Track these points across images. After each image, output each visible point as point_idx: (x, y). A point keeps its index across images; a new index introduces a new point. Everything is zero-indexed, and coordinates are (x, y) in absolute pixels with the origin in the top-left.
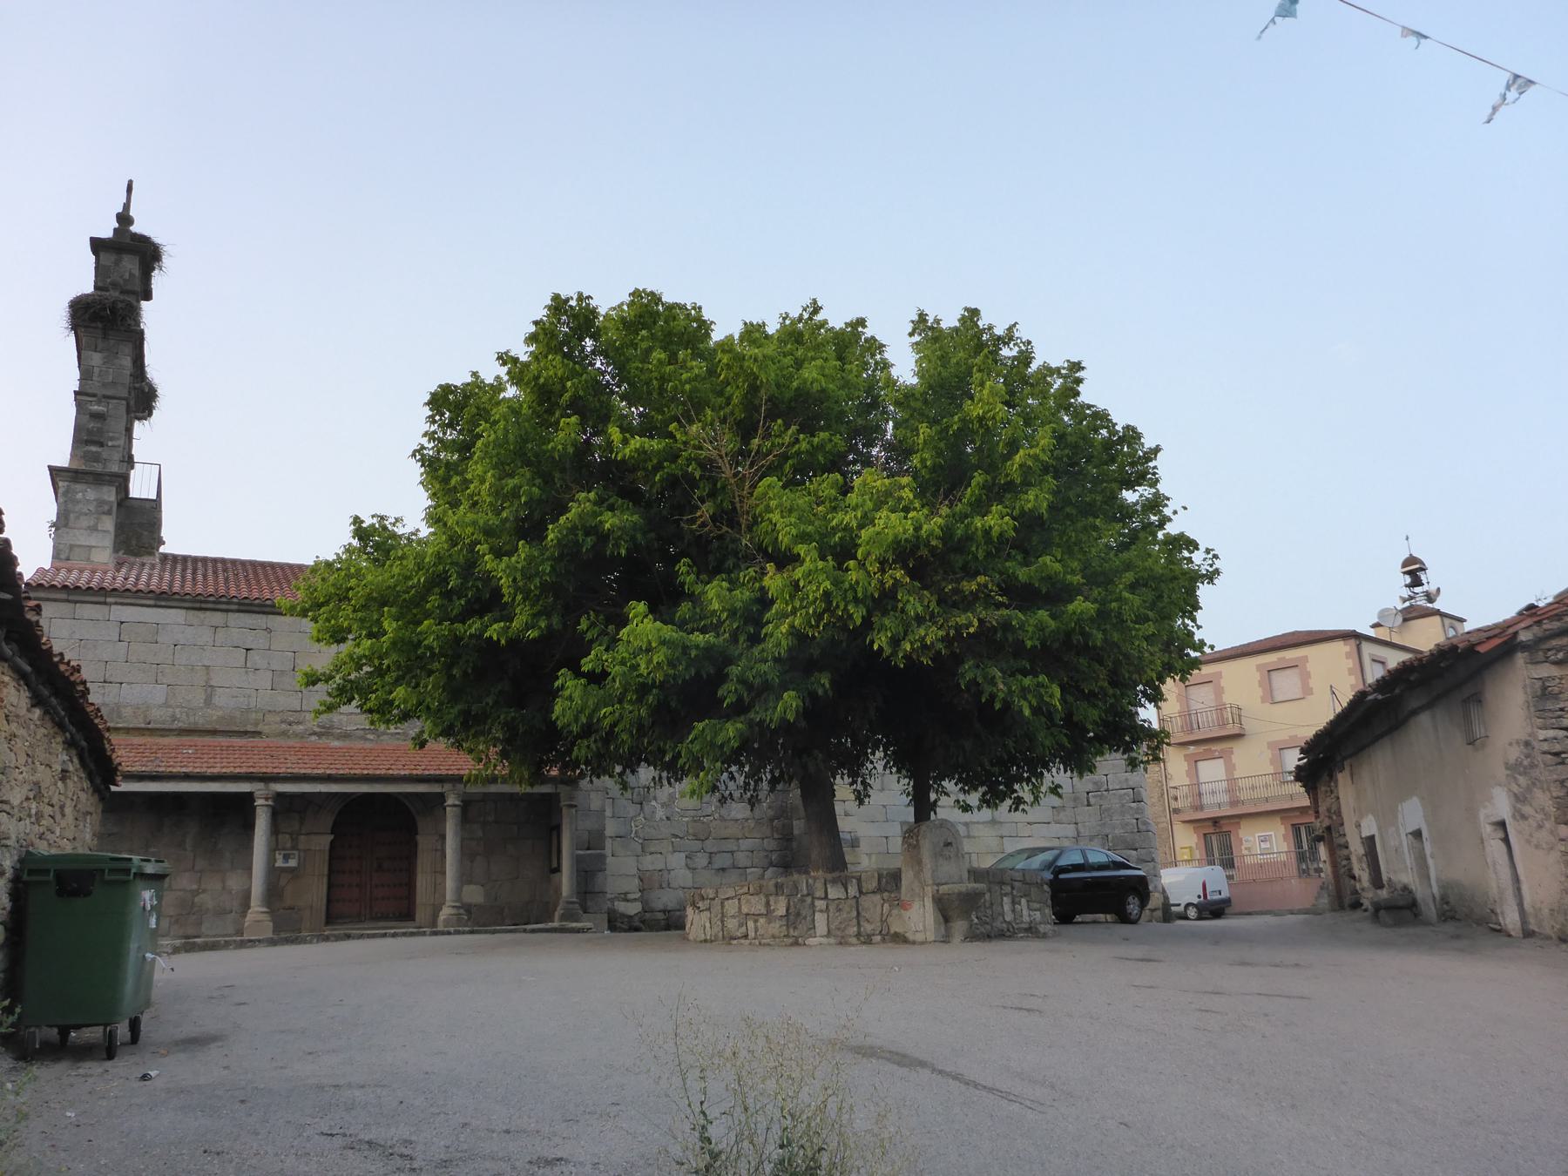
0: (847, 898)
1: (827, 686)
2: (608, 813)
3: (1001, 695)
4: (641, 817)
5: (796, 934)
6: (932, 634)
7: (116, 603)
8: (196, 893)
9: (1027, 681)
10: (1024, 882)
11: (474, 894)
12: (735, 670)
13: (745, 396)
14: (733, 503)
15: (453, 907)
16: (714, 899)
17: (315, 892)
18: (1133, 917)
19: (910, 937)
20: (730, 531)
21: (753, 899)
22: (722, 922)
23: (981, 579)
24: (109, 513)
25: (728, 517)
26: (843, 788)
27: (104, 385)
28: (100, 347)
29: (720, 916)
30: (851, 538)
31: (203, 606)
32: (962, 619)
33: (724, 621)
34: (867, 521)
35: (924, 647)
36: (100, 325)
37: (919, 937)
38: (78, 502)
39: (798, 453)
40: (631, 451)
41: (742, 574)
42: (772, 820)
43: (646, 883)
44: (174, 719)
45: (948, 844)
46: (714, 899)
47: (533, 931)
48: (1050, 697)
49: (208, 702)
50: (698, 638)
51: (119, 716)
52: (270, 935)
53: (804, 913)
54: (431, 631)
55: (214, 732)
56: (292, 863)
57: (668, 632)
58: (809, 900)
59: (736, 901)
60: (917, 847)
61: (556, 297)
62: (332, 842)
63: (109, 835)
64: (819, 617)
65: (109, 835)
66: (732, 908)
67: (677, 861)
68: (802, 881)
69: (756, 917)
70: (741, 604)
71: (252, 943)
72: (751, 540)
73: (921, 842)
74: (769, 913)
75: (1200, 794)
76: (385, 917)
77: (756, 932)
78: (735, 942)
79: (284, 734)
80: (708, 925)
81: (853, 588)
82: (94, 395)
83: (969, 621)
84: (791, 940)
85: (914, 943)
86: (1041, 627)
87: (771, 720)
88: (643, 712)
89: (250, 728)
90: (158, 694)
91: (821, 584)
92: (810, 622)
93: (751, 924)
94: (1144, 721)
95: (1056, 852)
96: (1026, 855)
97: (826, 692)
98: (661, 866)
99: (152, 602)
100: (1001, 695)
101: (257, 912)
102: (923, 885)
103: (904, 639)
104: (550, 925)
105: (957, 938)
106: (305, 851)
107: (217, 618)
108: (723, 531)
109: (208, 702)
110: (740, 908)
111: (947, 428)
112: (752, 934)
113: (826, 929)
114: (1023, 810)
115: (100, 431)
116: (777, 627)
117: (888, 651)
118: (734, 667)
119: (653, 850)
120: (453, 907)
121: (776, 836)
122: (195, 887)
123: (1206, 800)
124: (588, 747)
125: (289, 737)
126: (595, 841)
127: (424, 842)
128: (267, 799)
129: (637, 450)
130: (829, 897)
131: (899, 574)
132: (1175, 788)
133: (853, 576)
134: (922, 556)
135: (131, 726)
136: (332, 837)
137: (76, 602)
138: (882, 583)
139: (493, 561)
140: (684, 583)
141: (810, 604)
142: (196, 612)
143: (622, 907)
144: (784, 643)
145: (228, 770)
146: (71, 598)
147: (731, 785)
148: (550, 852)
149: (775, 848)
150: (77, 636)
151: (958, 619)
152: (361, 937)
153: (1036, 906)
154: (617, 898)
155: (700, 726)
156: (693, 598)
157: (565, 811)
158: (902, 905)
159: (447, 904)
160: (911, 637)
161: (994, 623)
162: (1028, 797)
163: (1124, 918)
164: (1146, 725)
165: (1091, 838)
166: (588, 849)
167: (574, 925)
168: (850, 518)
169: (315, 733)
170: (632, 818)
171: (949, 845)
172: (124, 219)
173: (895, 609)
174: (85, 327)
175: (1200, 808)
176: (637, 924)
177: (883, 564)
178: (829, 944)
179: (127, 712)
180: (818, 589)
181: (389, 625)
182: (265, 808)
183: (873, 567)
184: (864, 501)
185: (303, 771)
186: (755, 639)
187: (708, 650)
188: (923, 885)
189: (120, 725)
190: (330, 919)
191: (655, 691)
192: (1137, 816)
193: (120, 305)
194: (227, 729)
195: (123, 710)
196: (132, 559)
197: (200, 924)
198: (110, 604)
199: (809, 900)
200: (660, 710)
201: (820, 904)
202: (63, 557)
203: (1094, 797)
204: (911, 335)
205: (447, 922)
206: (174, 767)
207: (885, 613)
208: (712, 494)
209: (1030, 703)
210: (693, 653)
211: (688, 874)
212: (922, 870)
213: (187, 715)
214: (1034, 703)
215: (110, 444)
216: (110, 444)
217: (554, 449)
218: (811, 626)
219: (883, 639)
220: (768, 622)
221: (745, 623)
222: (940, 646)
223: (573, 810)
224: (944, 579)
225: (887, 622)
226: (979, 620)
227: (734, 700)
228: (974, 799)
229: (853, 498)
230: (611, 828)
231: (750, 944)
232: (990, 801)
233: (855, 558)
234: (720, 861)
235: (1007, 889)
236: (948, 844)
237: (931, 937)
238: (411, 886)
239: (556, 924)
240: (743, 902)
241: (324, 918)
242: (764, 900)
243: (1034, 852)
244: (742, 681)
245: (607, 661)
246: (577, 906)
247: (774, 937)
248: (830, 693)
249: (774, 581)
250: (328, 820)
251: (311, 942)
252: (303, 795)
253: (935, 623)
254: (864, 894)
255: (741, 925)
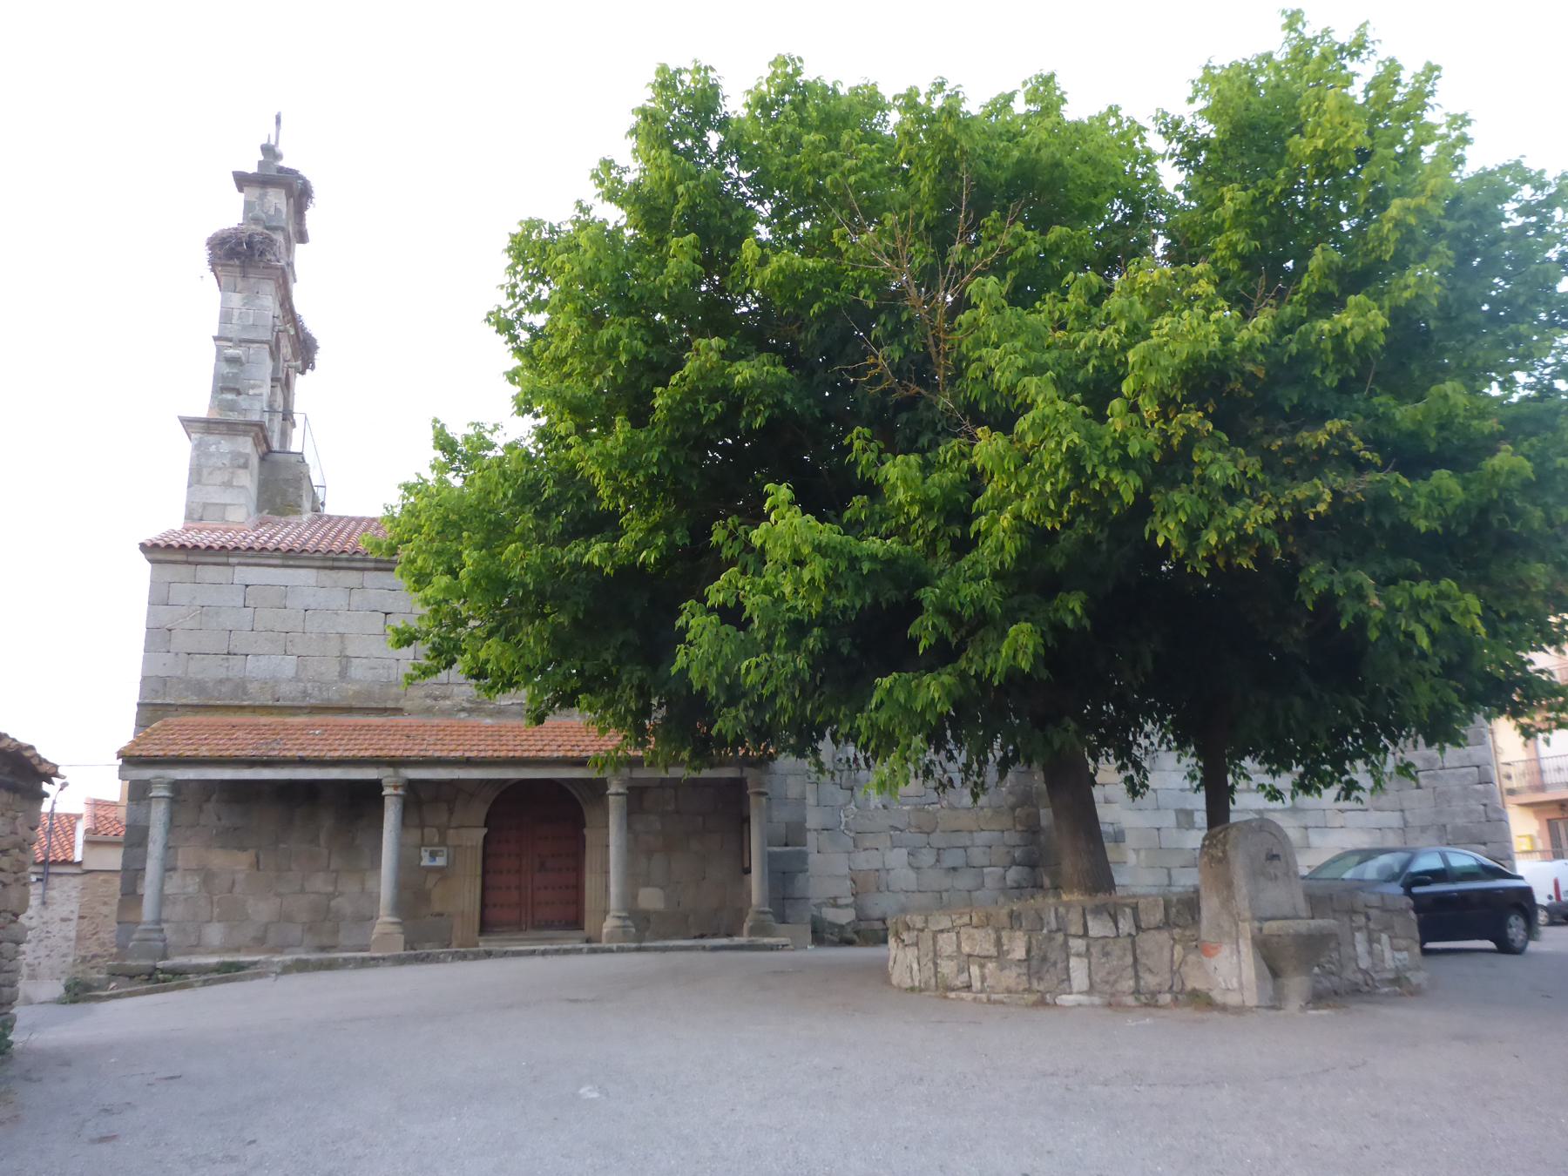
0: (1118, 936)
1: (1078, 611)
2: (811, 800)
3: (1377, 615)
4: (852, 806)
5: (1041, 988)
6: (1255, 516)
7: (240, 564)
8: (331, 896)
9: (1423, 590)
10: (1384, 909)
11: (651, 899)
12: (928, 595)
13: (937, 181)
14: (925, 346)
15: (619, 917)
16: (922, 930)
17: (466, 896)
18: (1517, 945)
19: (1218, 996)
20: (923, 391)
21: (978, 934)
22: (936, 964)
23: (1333, 425)
24: (245, 466)
25: (919, 368)
26: (1108, 776)
27: (245, 328)
28: (239, 288)
29: (931, 955)
30: (1111, 367)
31: (336, 564)
32: (1302, 491)
33: (916, 519)
34: (1137, 332)
35: (1243, 539)
36: (237, 262)
37: (1233, 999)
38: (212, 455)
39: (1025, 258)
40: (772, 272)
41: (941, 449)
42: (1013, 809)
43: (861, 885)
44: (305, 694)
45: (1273, 857)
46: (922, 930)
47: (715, 949)
48: (1462, 615)
49: (343, 674)
50: (874, 545)
51: (245, 693)
52: (400, 951)
53: (1052, 956)
54: (517, 558)
55: (349, 710)
56: (440, 861)
57: (828, 533)
58: (1060, 937)
59: (953, 935)
60: (1223, 860)
61: (663, 69)
62: (485, 837)
63: (235, 829)
64: (1063, 497)
65: (235, 829)
66: (947, 943)
67: (898, 858)
68: (1047, 904)
69: (983, 959)
70: (938, 492)
71: (374, 962)
72: (953, 398)
73: (1231, 854)
74: (1001, 955)
75: (1541, 772)
76: (549, 925)
77: (983, 982)
78: (952, 995)
79: (428, 711)
80: (915, 966)
81: (1121, 443)
82: (230, 340)
83: (1318, 494)
84: (1031, 998)
85: (1224, 1008)
86: (1438, 499)
87: (993, 672)
88: (801, 663)
89: (390, 704)
90: (288, 666)
91: (1062, 438)
92: (1047, 507)
93: (975, 970)
94: (1542, 671)
95: (1403, 856)
96: (1357, 858)
97: (1077, 619)
98: (879, 866)
99: (318, 563)
100: (1377, 615)
101: (385, 923)
102: (1236, 919)
103: (1206, 526)
104: (737, 940)
105: (1294, 1004)
106: (455, 847)
107: (352, 578)
108: (912, 392)
109: (343, 674)
110: (959, 946)
111: (1266, 193)
112: (977, 985)
113: (1086, 981)
114: (1358, 799)
115: (235, 376)
116: (995, 521)
117: (1179, 545)
118: (929, 589)
119: (867, 844)
120: (619, 917)
121: (1019, 828)
122: (330, 889)
123: (1550, 778)
124: (736, 717)
125: (434, 714)
126: (794, 834)
127: (590, 834)
128: (396, 787)
129: (781, 270)
130: (1091, 933)
131: (1194, 418)
132: (1509, 764)
133: (1117, 424)
134: (1233, 390)
135: (257, 703)
136: (485, 831)
137: (197, 564)
138: (1166, 437)
139: (579, 444)
140: (856, 463)
141: (1044, 478)
142: (327, 572)
143: (830, 914)
144: (1010, 547)
145: (351, 754)
146: (191, 559)
147: (951, 766)
148: (742, 842)
149: (1018, 842)
150: (198, 602)
151: (1295, 492)
152: (505, 954)
153: (1402, 943)
154: (825, 904)
155: (886, 682)
156: (873, 490)
157: (753, 800)
158: (1201, 948)
159: (612, 914)
160: (1218, 521)
161: (1359, 496)
162: (1365, 780)
163: (1506, 947)
164: (1544, 677)
165: (1424, 829)
166: (786, 845)
167: (766, 940)
168: (1110, 337)
169: (464, 710)
170: (841, 808)
171: (1276, 855)
172: (269, 151)
173: (1188, 479)
174: (222, 265)
175: (1542, 788)
176: (850, 935)
177: (1167, 406)
178: (1093, 1006)
179: (253, 688)
180: (1059, 444)
181: (470, 557)
182: (394, 798)
183: (1149, 408)
184: (1132, 304)
185: (437, 754)
186: (964, 546)
187: (891, 561)
188: (1236, 919)
189: (245, 703)
190: (485, 927)
191: (816, 631)
192: (1485, 801)
193: (257, 238)
194: (365, 705)
195: (249, 686)
196: (277, 518)
197: (336, 932)
198: (233, 565)
199: (1060, 937)
200: (823, 660)
201: (1077, 945)
202: (196, 516)
203: (1427, 777)
204: (1191, 100)
205: (611, 938)
206: (289, 750)
207: (1173, 485)
208: (894, 335)
209: (1427, 627)
210: (866, 567)
211: (912, 875)
212: (1234, 898)
213: (320, 690)
214: (1436, 625)
215: (251, 392)
216: (251, 392)
217: (662, 285)
218: (1051, 513)
219: (1172, 526)
220: (980, 513)
221: (948, 522)
222: (1269, 536)
223: (764, 799)
224: (1266, 432)
225: (1177, 497)
226: (1333, 491)
227: (933, 641)
228: (1285, 782)
229: (1114, 303)
230: (813, 819)
231: (975, 999)
232: (1304, 786)
233: (1119, 394)
234: (951, 859)
235: (1361, 920)
236: (1273, 857)
237: (1251, 999)
238: (578, 888)
239: (741, 940)
240: (963, 937)
241: (477, 927)
242: (993, 936)
243: (1367, 855)
244: (945, 611)
245: (743, 588)
246: (770, 917)
247: (1009, 991)
248: (1087, 623)
249: (988, 446)
250: (480, 811)
251: (444, 961)
252: (451, 782)
253: (1258, 500)
254: (1144, 931)
255: (961, 971)
